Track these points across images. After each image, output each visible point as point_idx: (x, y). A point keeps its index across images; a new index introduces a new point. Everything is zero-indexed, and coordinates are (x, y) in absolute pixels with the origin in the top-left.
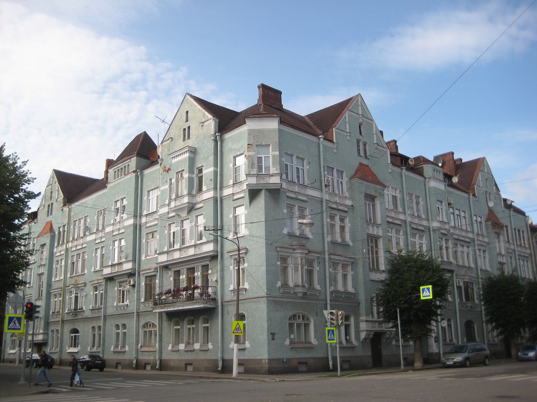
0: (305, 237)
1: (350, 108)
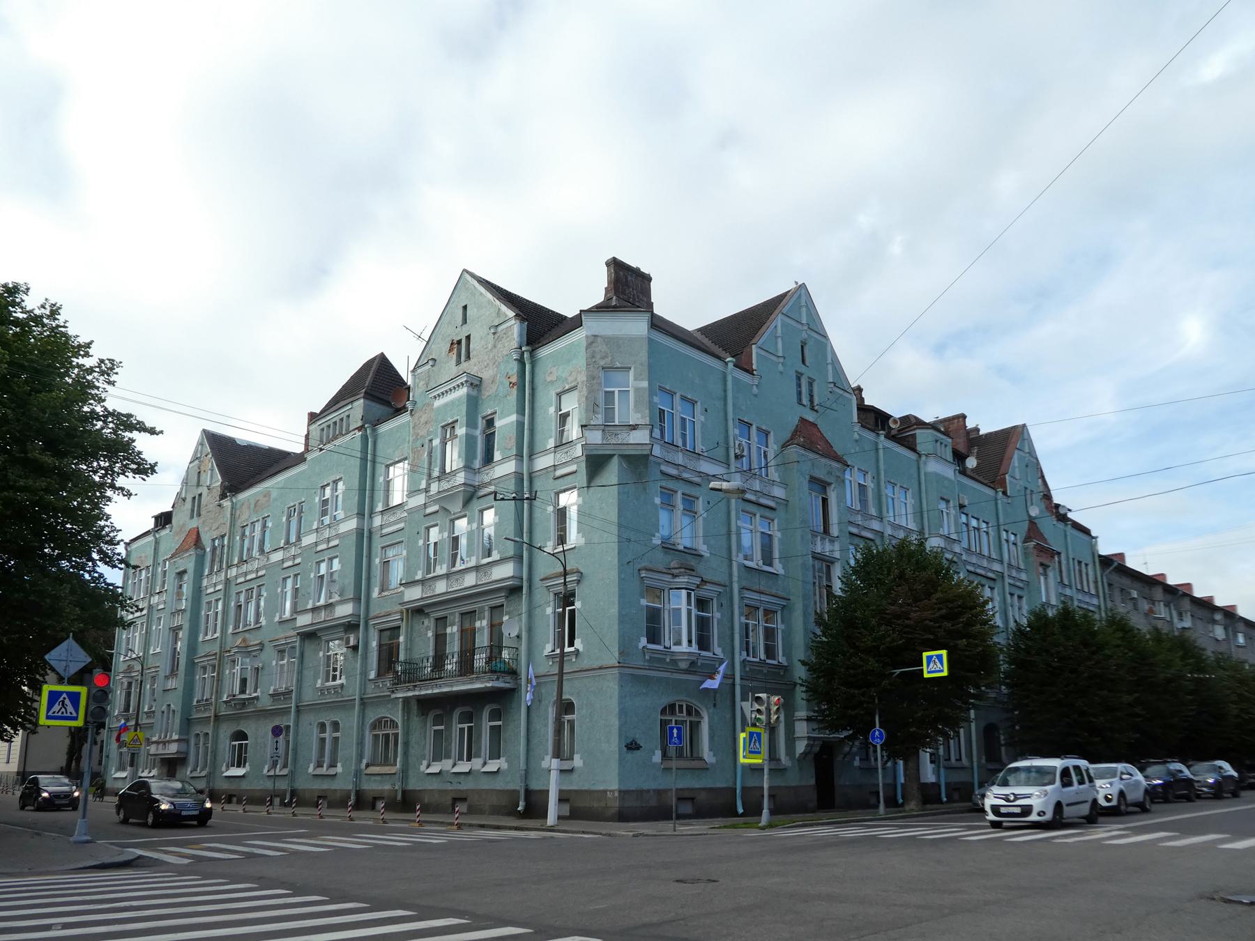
0: (694, 552)
1: (785, 311)
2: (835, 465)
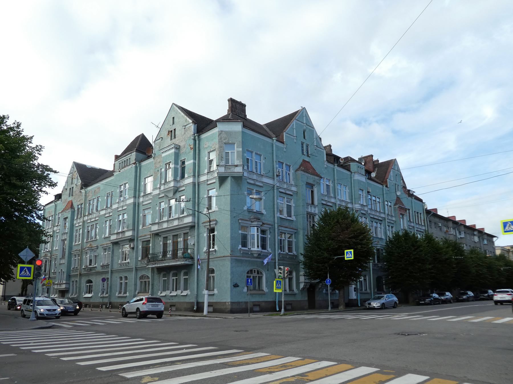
1: (297, 118)
2: (316, 177)
